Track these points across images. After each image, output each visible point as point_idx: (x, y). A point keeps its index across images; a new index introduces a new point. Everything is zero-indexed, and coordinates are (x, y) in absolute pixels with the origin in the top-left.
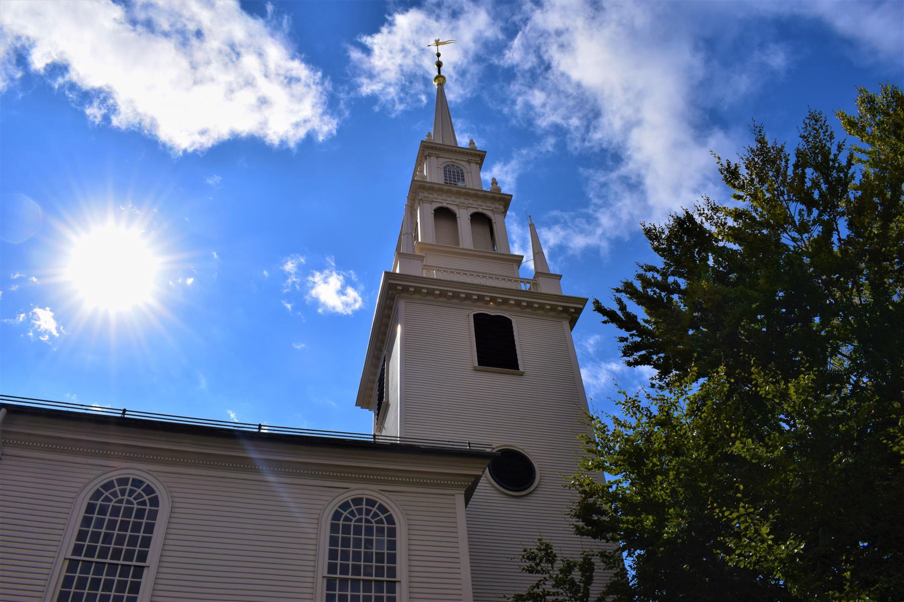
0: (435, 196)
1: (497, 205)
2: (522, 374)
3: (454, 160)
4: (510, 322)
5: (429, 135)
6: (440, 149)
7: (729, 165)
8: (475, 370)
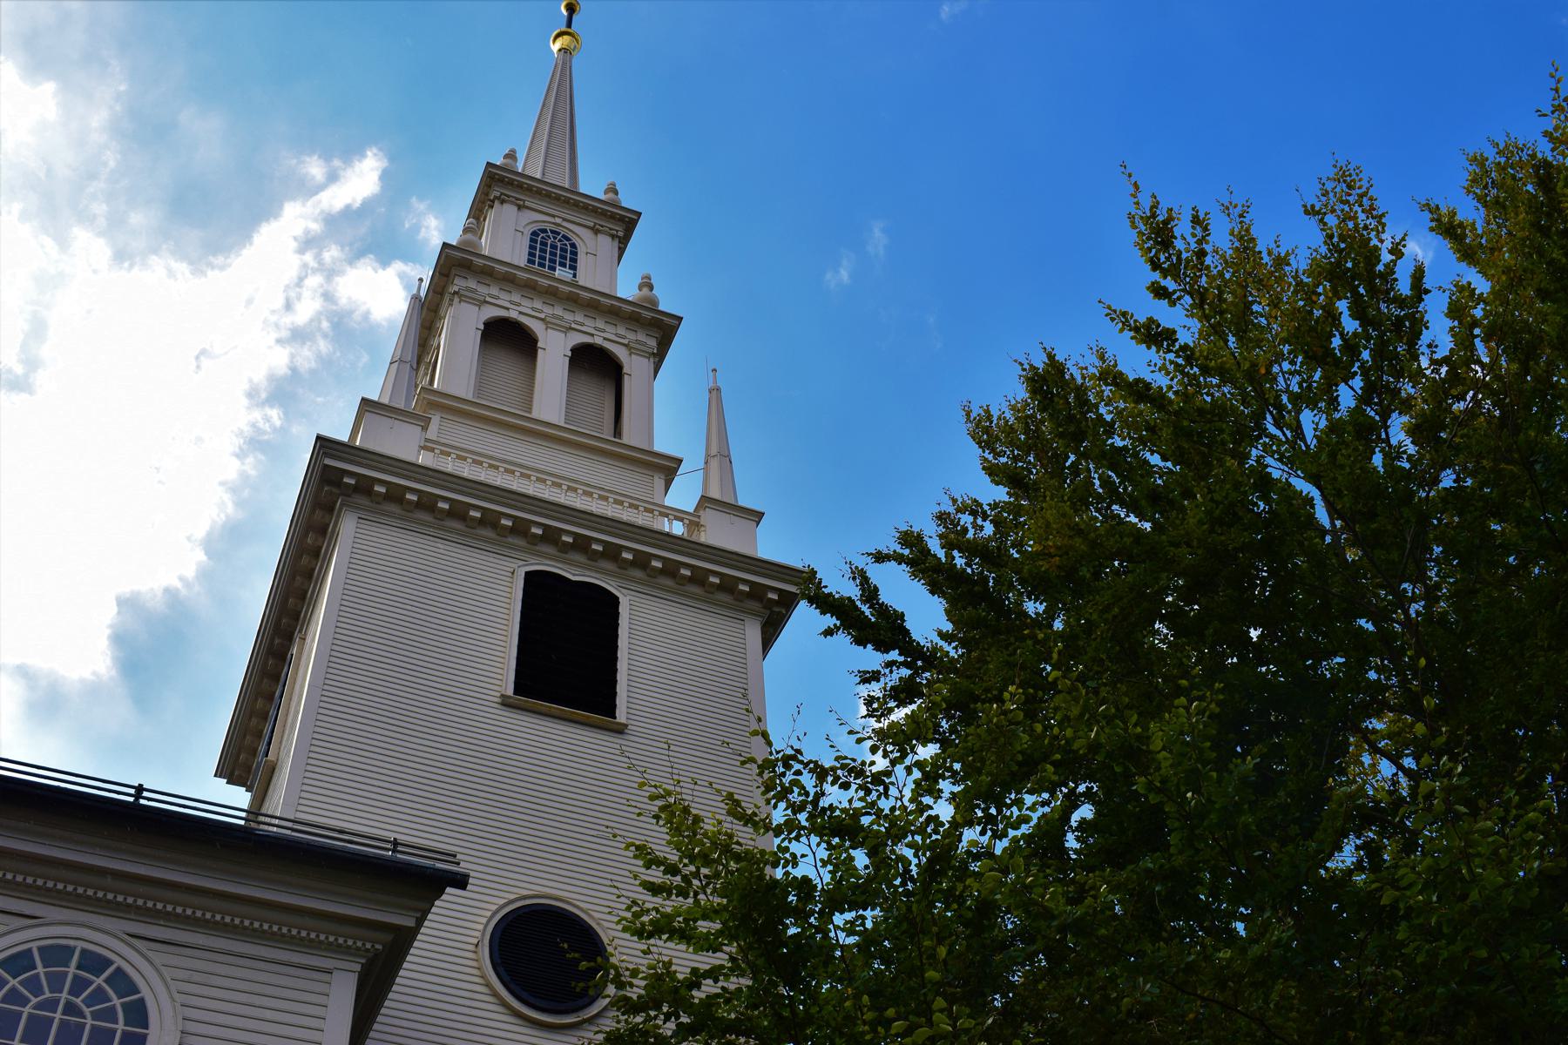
0: (494, 291)
1: (641, 337)
2: (620, 730)
3: (558, 221)
4: (615, 601)
5: (511, 155)
6: (529, 189)
7: (1155, 206)
8: (503, 704)
